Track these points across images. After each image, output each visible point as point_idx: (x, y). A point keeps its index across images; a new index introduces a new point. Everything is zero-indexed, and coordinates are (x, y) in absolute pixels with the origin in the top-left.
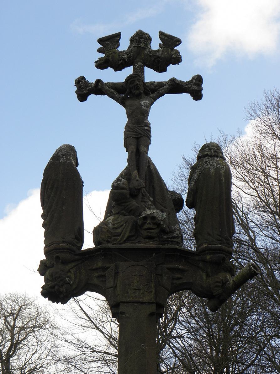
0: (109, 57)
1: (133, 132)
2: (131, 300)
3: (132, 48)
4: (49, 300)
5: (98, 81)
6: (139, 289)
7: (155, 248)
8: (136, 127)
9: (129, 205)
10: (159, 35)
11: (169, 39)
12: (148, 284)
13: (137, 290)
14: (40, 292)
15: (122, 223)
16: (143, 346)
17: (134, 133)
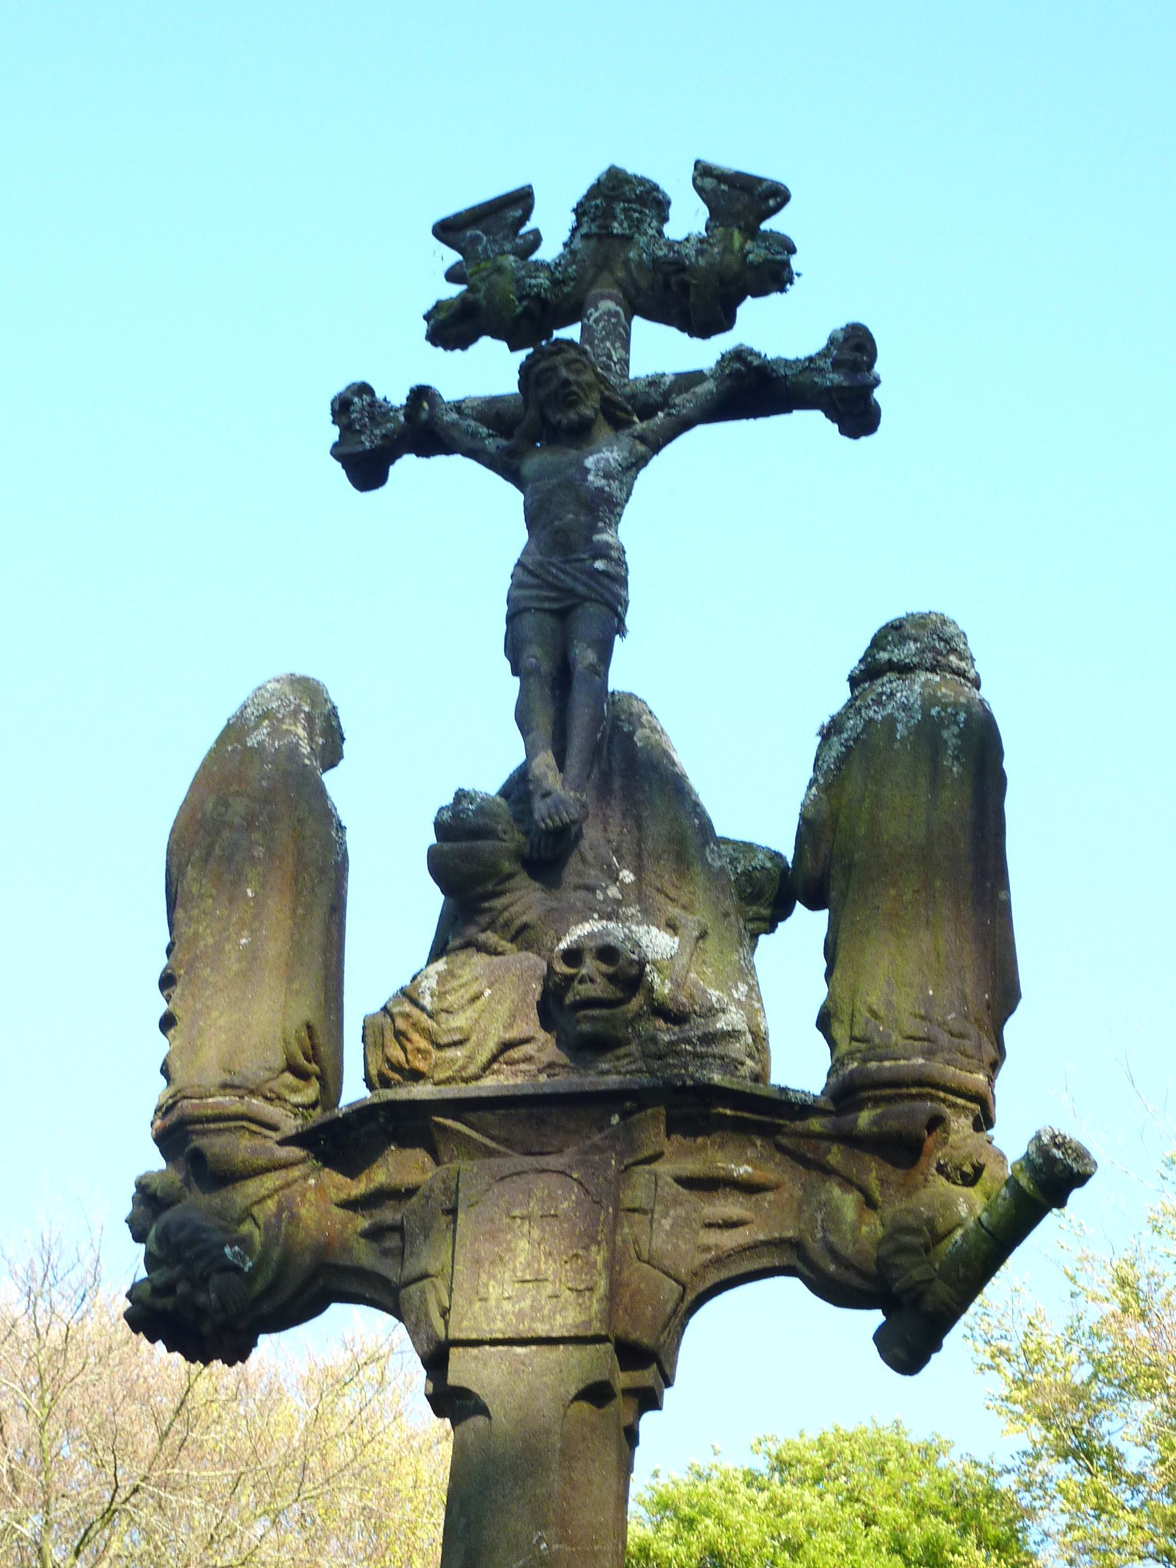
0: (478, 291)
1: (541, 588)
2: (500, 1331)
3: (578, 244)
4: (170, 1350)
5: (421, 394)
6: (537, 1280)
7: (616, 1087)
8: (553, 565)
9: (511, 904)
10: (694, 180)
11: (735, 187)
12: (581, 1252)
13: (530, 1285)
14: (907, 1379)
15: (474, 988)
16: (540, 1540)
17: (545, 594)
